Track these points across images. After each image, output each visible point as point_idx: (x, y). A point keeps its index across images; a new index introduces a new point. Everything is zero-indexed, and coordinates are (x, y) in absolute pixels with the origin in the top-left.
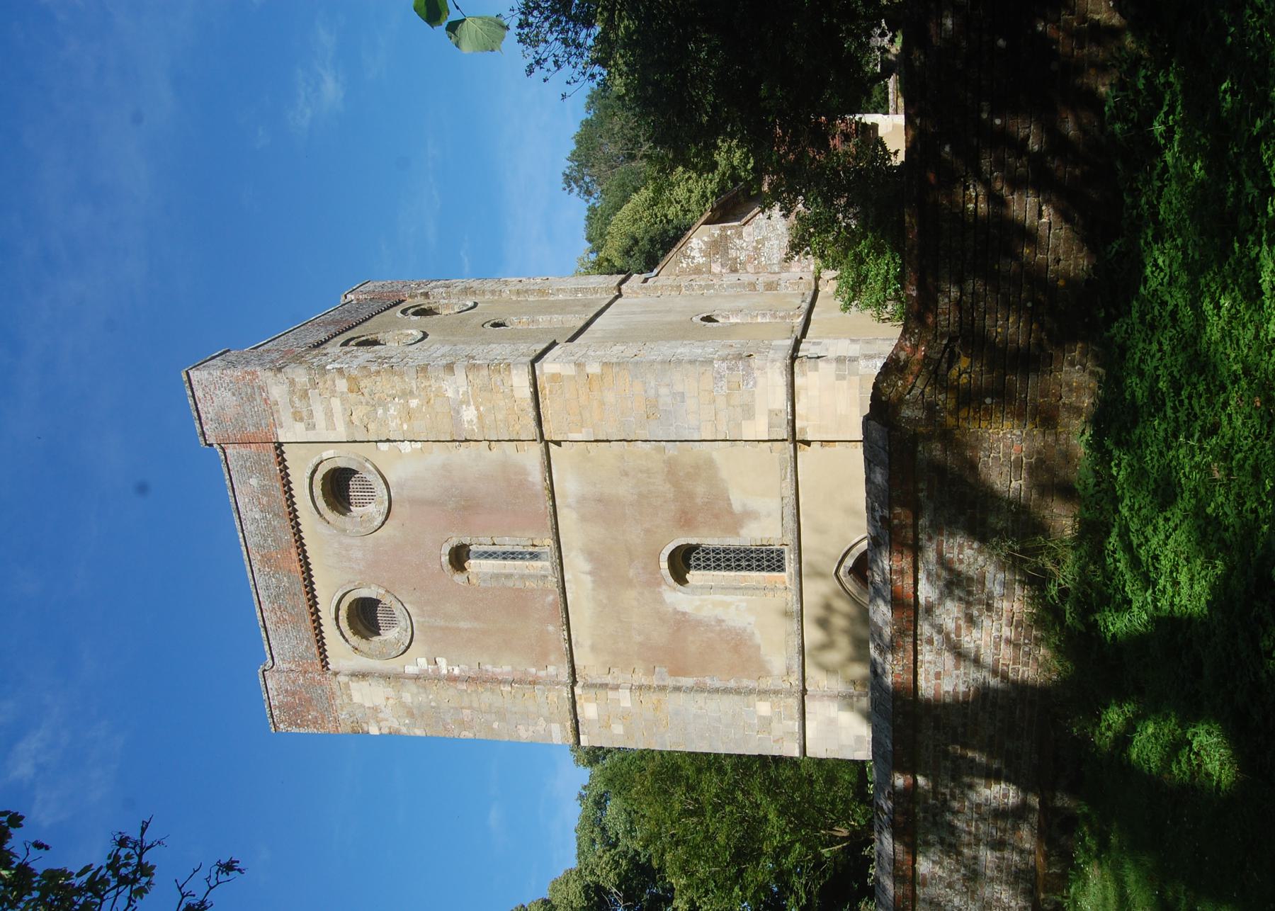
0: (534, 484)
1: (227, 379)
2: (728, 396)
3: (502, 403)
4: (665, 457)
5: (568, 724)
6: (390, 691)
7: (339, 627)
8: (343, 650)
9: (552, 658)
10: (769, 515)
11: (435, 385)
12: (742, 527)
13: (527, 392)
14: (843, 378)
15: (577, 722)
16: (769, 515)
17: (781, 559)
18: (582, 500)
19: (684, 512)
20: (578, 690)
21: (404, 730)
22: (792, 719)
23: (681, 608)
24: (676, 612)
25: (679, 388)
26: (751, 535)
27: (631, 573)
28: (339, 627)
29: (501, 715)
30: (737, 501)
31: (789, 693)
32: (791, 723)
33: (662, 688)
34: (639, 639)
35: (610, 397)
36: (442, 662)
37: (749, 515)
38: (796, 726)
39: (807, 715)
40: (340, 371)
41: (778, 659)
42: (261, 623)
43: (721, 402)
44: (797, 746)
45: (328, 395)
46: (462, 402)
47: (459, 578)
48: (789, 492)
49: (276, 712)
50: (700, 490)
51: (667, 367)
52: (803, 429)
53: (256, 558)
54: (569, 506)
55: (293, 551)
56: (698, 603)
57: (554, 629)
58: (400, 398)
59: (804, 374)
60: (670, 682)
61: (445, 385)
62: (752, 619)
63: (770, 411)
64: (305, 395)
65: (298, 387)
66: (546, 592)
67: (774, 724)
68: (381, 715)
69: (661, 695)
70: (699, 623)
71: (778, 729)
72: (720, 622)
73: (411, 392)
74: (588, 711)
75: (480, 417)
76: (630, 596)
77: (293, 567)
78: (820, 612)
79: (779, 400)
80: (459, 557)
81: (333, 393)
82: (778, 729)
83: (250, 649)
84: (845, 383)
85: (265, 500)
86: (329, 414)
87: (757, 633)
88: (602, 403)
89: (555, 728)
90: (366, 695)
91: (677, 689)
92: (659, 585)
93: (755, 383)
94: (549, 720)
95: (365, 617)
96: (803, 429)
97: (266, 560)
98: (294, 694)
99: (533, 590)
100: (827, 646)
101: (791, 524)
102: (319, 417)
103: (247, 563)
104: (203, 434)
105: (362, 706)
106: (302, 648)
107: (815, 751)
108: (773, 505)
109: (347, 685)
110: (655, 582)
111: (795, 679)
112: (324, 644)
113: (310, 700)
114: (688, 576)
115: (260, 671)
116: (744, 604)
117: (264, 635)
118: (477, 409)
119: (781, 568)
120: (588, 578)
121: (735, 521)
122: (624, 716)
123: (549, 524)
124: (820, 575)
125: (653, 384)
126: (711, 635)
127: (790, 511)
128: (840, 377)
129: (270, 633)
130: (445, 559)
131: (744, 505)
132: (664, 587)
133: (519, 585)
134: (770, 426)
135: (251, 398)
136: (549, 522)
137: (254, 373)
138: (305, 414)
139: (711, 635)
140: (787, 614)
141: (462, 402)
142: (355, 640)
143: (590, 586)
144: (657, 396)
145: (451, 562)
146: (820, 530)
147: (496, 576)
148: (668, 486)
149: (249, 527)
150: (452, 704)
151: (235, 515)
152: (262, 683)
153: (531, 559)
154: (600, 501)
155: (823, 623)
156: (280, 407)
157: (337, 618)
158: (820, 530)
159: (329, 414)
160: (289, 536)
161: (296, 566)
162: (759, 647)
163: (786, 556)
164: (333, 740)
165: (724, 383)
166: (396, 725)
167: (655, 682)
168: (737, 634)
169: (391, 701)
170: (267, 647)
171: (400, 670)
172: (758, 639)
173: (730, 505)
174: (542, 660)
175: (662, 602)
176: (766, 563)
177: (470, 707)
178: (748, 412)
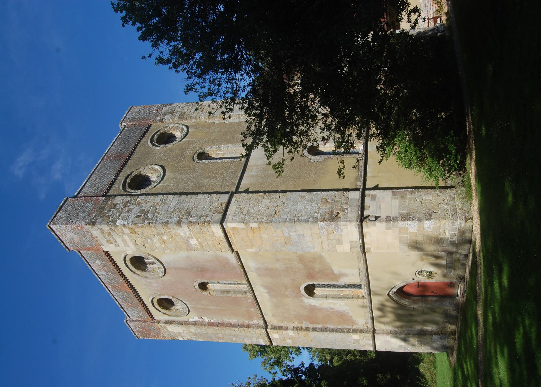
0: (233, 264)
1: (70, 229)
2: (327, 236)
3: (209, 238)
7: (155, 307)
8: (159, 315)
11: (173, 232)
12: (340, 279)
13: (222, 234)
14: (390, 229)
18: (258, 270)
20: (269, 330)
21: (194, 339)
23: (313, 304)
25: (301, 232)
27: (287, 293)
30: (336, 270)
31: (367, 332)
33: (307, 329)
35: (265, 236)
40: (124, 225)
45: (121, 234)
46: (189, 238)
47: (205, 293)
48: (363, 267)
49: (137, 333)
50: (317, 266)
51: (293, 224)
54: (252, 271)
55: (125, 285)
58: (157, 236)
59: (368, 227)
60: (311, 326)
62: (348, 308)
63: (351, 242)
64: (110, 234)
65: (105, 231)
66: (247, 298)
69: (308, 332)
72: (332, 309)
73: (162, 234)
75: (200, 243)
77: (127, 290)
80: (203, 286)
81: (124, 234)
83: (118, 316)
84: (391, 231)
85: (106, 268)
86: (125, 242)
87: (350, 312)
88: (261, 238)
90: (173, 330)
91: (314, 329)
93: (342, 231)
95: (166, 304)
97: (114, 287)
98: (142, 328)
99: (241, 298)
102: (119, 241)
104: (67, 247)
109: (165, 326)
111: (370, 325)
113: (150, 330)
114: (315, 291)
115: (125, 321)
117: (122, 310)
118: (197, 240)
120: (267, 294)
121: (354, 323)
122: (291, 338)
128: (387, 229)
133: (234, 295)
135: (84, 235)
136: (244, 276)
137: (81, 226)
138: (112, 241)
142: (163, 311)
144: (290, 236)
146: (377, 280)
147: (223, 292)
148: (300, 265)
154: (267, 269)
156: (99, 238)
158: (377, 280)
159: (125, 242)
160: (121, 280)
162: (352, 317)
164: (165, 342)
166: (190, 338)
167: (304, 326)
171: (187, 320)
172: (351, 314)
174: (251, 318)
175: (304, 302)
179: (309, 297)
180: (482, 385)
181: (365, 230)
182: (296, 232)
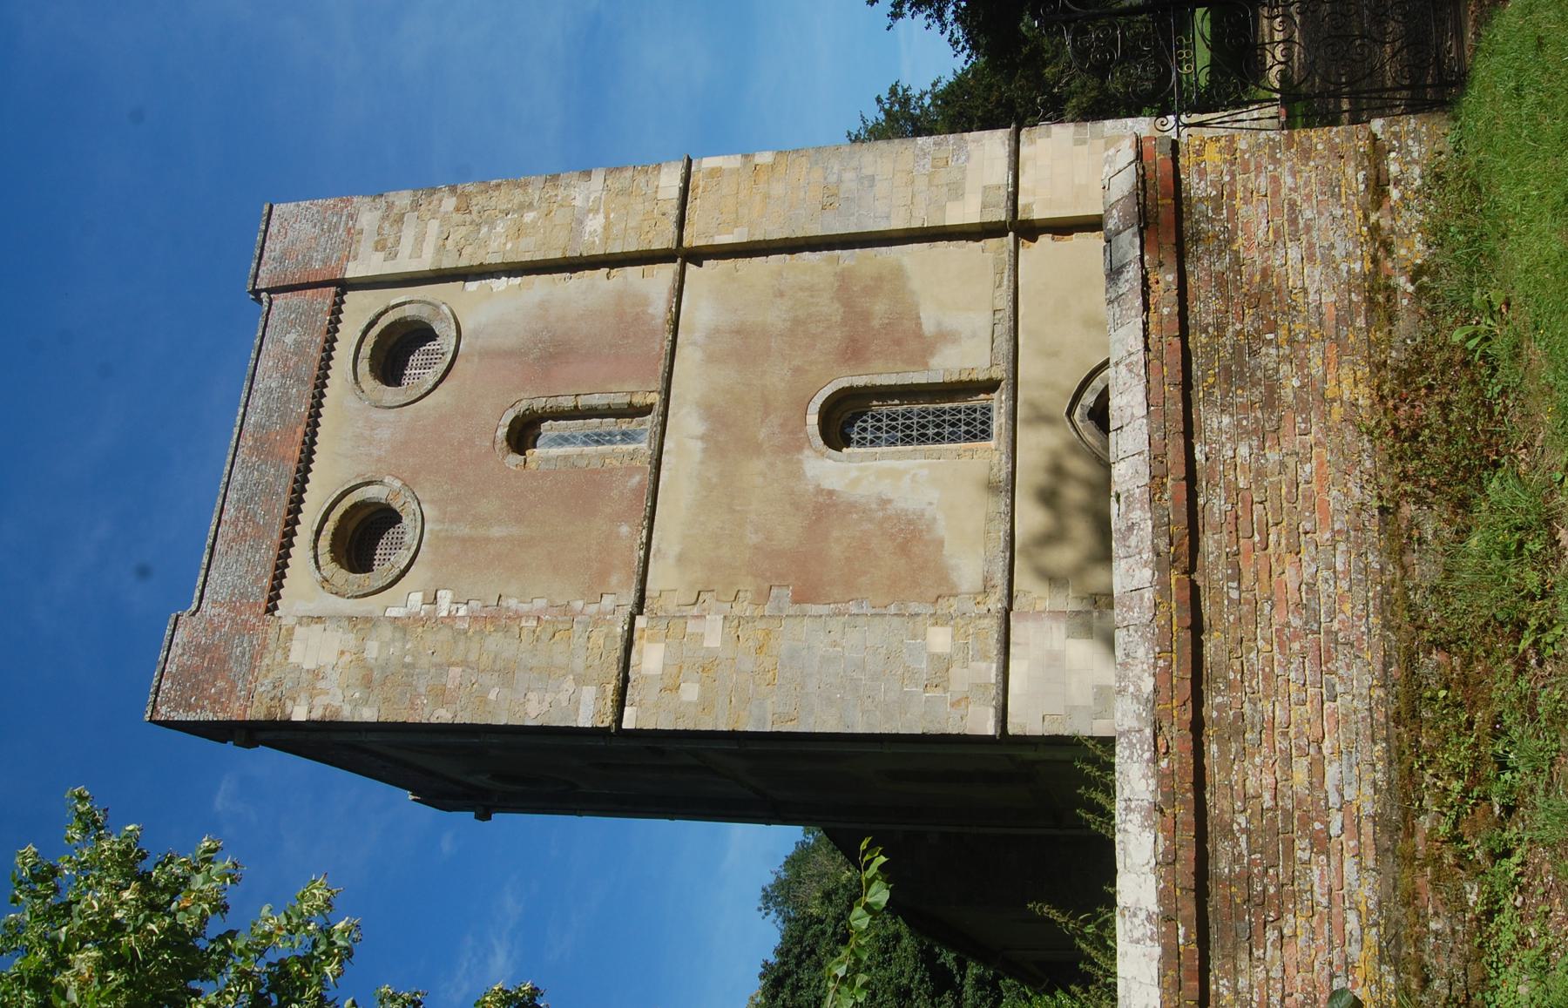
0: (653, 317)
2: (930, 176)
4: (838, 269)
5: (610, 688)
6: (351, 640)
7: (315, 547)
9: (614, 580)
10: (974, 335)
12: (932, 354)
13: (675, 193)
14: (1084, 142)
15: (626, 680)
16: (974, 335)
17: (986, 422)
18: (714, 333)
19: (853, 340)
20: (640, 622)
22: (985, 657)
23: (827, 484)
24: (819, 491)
26: (946, 366)
27: (762, 434)
28: (315, 547)
29: (506, 674)
32: (983, 665)
34: (753, 538)
36: (445, 597)
37: (947, 336)
38: (992, 671)
39: (1012, 650)
41: (971, 564)
42: (210, 541)
43: (921, 183)
44: (992, 711)
46: (590, 211)
48: (1005, 303)
50: (880, 308)
52: (1028, 206)
53: (247, 441)
54: (694, 343)
56: (854, 474)
57: (628, 532)
61: (573, 192)
64: (400, 219)
66: (630, 471)
67: (955, 671)
68: (321, 685)
70: (852, 506)
71: (961, 679)
72: (884, 503)
74: (650, 658)
76: (754, 470)
78: (1041, 478)
79: (1001, 175)
82: (961, 679)
84: (1085, 148)
88: (767, 196)
89: (589, 693)
92: (800, 449)
93: (968, 159)
94: (580, 681)
96: (1028, 206)
100: (1052, 538)
101: (1004, 346)
103: (231, 451)
104: (256, 276)
105: (298, 667)
106: (251, 578)
107: (1026, 721)
108: (982, 320)
110: (796, 444)
112: (283, 576)
116: (926, 472)
118: (607, 217)
119: (985, 434)
120: (699, 445)
122: (708, 666)
123: (661, 369)
124: (1043, 418)
125: (835, 170)
126: (867, 526)
127: (1004, 327)
128: (1080, 142)
129: (216, 556)
130: (502, 431)
131: (939, 324)
132: (807, 452)
134: (984, 206)
139: (867, 526)
140: (992, 487)
141: (590, 211)
143: (698, 456)
145: (509, 437)
149: (258, 401)
150: (436, 659)
151: (246, 384)
152: (168, 632)
153: (622, 441)
155: (1048, 498)
157: (318, 533)
161: (295, 452)
163: (995, 414)
165: (928, 162)
168: (910, 522)
169: (347, 658)
170: (201, 580)
172: (942, 529)
173: (919, 325)
176: (964, 428)
177: (464, 663)
178: (956, 191)
179: (825, 448)
180: (1154, 996)
181: (1023, 151)
182: (858, 169)
